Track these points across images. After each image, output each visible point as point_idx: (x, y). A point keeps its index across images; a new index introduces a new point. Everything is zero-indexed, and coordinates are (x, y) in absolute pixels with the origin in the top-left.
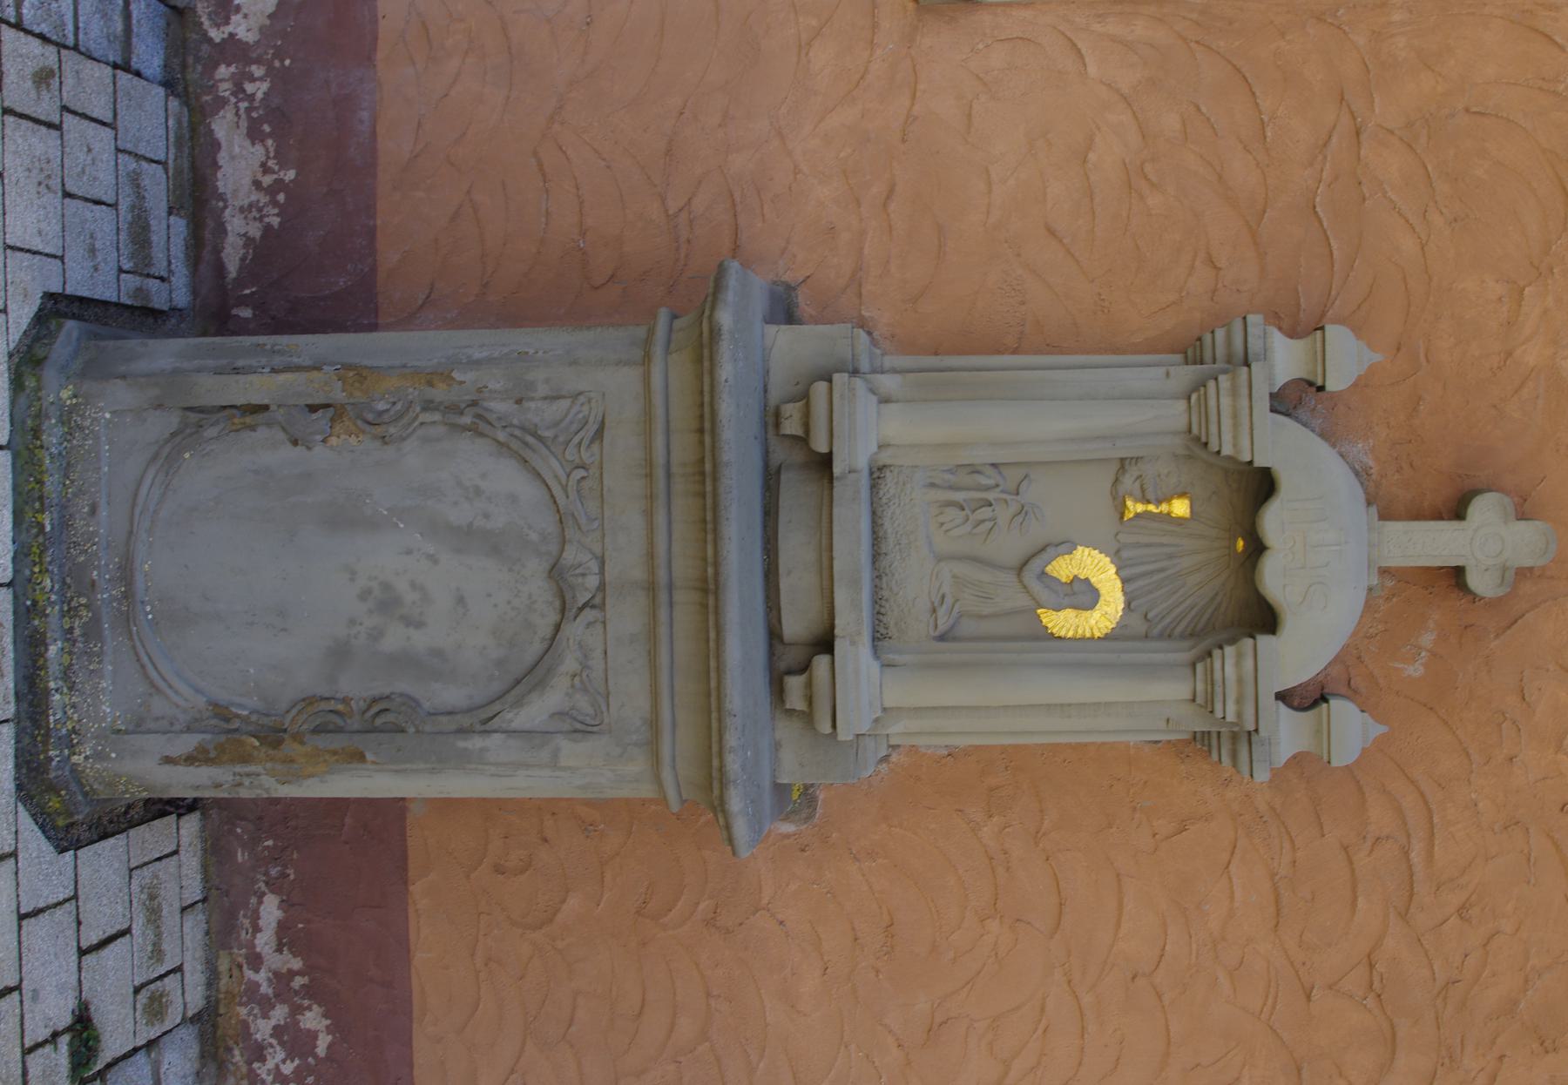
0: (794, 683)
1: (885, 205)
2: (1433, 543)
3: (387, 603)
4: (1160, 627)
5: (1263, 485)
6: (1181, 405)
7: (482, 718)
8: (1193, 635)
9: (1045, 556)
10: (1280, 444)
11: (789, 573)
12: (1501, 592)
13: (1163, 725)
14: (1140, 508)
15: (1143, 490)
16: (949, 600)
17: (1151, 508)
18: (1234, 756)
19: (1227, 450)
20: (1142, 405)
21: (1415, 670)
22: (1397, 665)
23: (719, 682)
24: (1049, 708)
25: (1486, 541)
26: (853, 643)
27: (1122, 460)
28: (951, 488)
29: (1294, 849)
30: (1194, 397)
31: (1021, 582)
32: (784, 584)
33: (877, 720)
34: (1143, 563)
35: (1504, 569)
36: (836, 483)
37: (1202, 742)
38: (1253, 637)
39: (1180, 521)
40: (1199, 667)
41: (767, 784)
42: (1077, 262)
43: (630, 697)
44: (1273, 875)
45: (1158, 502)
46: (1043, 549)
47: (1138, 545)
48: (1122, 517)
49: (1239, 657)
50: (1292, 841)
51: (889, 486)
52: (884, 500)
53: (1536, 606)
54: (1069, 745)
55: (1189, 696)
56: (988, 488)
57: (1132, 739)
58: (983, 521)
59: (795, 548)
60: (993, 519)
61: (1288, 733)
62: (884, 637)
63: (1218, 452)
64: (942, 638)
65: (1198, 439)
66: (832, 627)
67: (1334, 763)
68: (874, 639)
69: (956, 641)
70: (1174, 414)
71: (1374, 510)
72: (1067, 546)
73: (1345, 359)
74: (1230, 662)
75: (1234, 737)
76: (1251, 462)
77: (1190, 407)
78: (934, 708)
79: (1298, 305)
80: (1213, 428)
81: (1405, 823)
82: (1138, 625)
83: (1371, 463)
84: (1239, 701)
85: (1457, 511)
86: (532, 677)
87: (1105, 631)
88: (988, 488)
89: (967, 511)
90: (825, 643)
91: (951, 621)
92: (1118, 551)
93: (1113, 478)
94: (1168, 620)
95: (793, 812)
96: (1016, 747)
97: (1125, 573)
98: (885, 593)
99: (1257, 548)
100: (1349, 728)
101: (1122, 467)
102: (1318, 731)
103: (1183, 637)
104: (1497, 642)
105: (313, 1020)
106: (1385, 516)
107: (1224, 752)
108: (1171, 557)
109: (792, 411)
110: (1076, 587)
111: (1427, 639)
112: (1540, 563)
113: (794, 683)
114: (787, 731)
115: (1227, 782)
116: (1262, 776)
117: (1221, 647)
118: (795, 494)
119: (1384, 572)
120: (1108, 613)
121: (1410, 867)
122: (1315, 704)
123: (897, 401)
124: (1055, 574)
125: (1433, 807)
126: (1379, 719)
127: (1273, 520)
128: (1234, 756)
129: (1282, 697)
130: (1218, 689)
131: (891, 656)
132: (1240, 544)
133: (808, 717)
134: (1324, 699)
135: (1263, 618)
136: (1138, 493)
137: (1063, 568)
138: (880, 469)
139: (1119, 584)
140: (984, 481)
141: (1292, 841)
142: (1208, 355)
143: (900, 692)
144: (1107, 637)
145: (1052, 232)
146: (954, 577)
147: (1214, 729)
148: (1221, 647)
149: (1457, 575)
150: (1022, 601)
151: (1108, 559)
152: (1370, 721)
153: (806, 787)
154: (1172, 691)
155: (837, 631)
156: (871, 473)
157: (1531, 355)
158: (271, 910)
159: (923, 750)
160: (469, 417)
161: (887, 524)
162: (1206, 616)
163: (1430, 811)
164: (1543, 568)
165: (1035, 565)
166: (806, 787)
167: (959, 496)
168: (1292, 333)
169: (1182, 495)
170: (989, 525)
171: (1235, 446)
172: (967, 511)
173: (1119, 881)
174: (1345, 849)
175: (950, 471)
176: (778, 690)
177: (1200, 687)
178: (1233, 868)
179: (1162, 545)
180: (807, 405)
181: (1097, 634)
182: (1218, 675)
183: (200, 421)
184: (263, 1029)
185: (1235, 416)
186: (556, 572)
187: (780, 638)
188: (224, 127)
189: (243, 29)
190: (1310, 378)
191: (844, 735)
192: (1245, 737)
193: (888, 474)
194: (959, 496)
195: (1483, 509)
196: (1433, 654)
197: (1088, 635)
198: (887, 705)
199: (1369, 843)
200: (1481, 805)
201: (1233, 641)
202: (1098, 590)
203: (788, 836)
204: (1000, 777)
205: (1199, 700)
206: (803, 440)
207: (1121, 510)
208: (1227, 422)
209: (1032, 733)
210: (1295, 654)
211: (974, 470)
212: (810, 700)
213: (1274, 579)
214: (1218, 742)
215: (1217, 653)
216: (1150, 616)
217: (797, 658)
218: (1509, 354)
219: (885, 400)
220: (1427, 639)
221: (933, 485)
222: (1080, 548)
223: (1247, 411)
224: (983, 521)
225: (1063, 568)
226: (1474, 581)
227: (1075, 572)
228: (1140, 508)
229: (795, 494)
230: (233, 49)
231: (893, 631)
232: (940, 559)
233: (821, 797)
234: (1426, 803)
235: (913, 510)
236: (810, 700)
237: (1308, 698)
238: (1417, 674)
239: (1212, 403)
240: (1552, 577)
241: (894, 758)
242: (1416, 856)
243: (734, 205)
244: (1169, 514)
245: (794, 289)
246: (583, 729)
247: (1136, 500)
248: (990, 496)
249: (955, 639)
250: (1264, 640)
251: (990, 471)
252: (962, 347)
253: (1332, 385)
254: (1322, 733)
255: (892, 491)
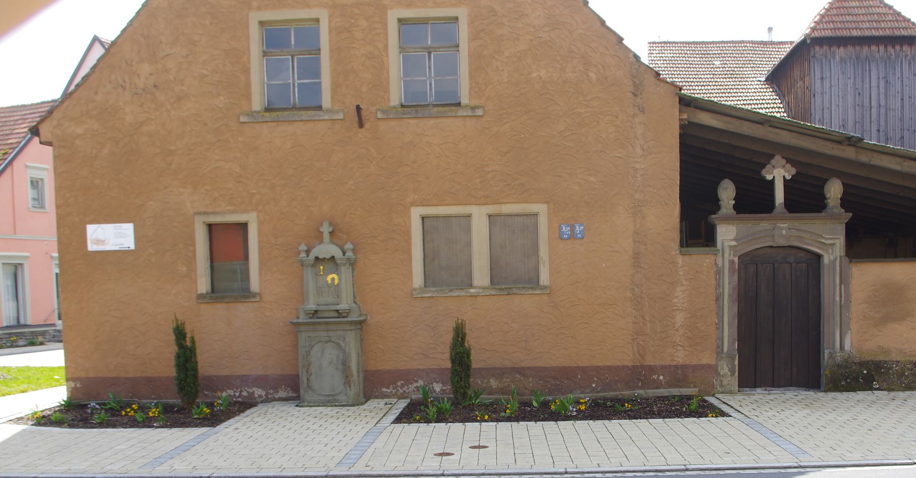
2: (326, 237)
3: (330, 363)
5: (317, 258)
7: (344, 351)
10: (312, 256)
20: (309, 273)
43: (340, 333)
59: (326, 315)
61: (349, 254)
69: (338, 296)
70: (309, 269)
73: (303, 247)
86: (338, 344)
90: (337, 311)
100: (349, 246)
105: (399, 384)
118: (320, 315)
120: (335, 276)
127: (321, 257)
137: (330, 282)
158: (384, 390)
160: (308, 353)
183: (309, 387)
184: (401, 391)
186: (326, 342)
188: (277, 397)
189: (264, 394)
195: (321, 230)
202: (332, 277)
210: (338, 253)
213: (328, 256)
214: (352, 264)
225: (330, 282)
229: (320, 315)
230: (266, 395)
246: (345, 339)
252: (303, 297)
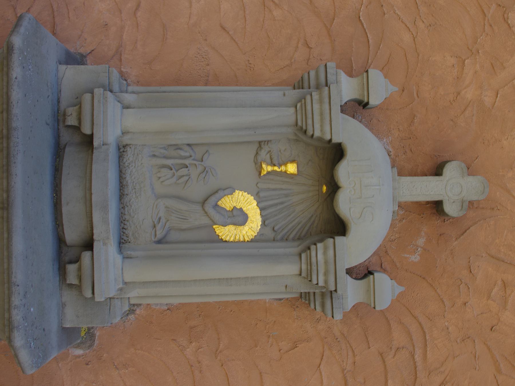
0: (72, 268)
1: (135, 14)
2: (426, 189)
4: (281, 234)
6: (292, 110)
8: (300, 238)
9: (217, 195)
11: (67, 204)
12: (461, 214)
13: (283, 289)
14: (270, 168)
15: (271, 159)
16: (163, 220)
17: (276, 168)
18: (323, 306)
19: (317, 134)
20: (270, 111)
21: (415, 258)
22: (406, 255)
23: (9, 265)
24: (220, 280)
25: (453, 187)
26: (105, 244)
27: (260, 143)
28: (166, 157)
29: (354, 356)
30: (299, 105)
31: (204, 210)
32: (65, 210)
33: (121, 290)
34: (272, 200)
35: (463, 202)
36: (94, 151)
37: (305, 298)
38: (334, 238)
39: (292, 175)
40: (303, 256)
41: (54, 327)
42: (236, 43)
44: (343, 370)
45: (280, 166)
46: (217, 192)
47: (269, 189)
48: (260, 174)
49: (326, 249)
50: (353, 352)
51: (129, 157)
52: (126, 164)
53: (475, 223)
54: (233, 302)
55: (298, 272)
56: (186, 158)
57: (267, 298)
58: (183, 176)
59: (71, 188)
60: (188, 175)
61: (352, 292)
62: (126, 242)
63: (313, 135)
64: (159, 242)
65: (302, 128)
66: (93, 235)
67: (378, 308)
68: (120, 243)
69: (166, 243)
70: (288, 115)
71: (395, 170)
72: (230, 190)
73: (380, 90)
74: (320, 252)
75: (323, 295)
76: (330, 140)
77: (296, 111)
78: (154, 282)
79: (352, 67)
80: (310, 121)
81: (412, 340)
82: (270, 234)
83: (390, 150)
84: (326, 274)
85: (437, 171)
87: (251, 237)
88: (186, 158)
89: (174, 170)
90: (89, 245)
91: (164, 233)
92: (258, 193)
93: (255, 152)
94: (286, 231)
95: (82, 343)
96: (205, 303)
97: (263, 204)
98: (127, 217)
99: (334, 188)
100: (385, 288)
101: (260, 146)
102: (368, 291)
103: (294, 240)
104: (456, 242)
106: (400, 174)
107: (317, 303)
108: (287, 196)
109: (72, 111)
110: (235, 213)
111: (421, 241)
112: (481, 198)
113: (72, 268)
114: (68, 296)
115: (318, 320)
116: (338, 316)
117: (315, 244)
119: (400, 206)
121: (415, 363)
122: (365, 276)
123: (134, 108)
124: (223, 206)
125: (426, 331)
126: (400, 283)
127: (344, 172)
128: (323, 306)
129: (349, 272)
130: (314, 268)
131: (129, 252)
132: (325, 188)
133: (79, 288)
134: (370, 273)
135: (339, 227)
136: (269, 160)
138: (124, 147)
139: (258, 211)
140: (183, 153)
141: (353, 352)
142: (306, 84)
143: (132, 274)
144: (252, 241)
145: (224, 29)
146: (166, 207)
147: (312, 291)
148: (315, 244)
149: (437, 206)
150: (205, 221)
151: (252, 197)
152: (396, 284)
153: (89, 329)
154: (288, 269)
155: (94, 237)
156: (119, 149)
157: (470, 94)
159: (154, 307)
161: (128, 178)
162: (306, 228)
163: (424, 333)
164: (478, 201)
165: (212, 200)
166: (89, 329)
167: (169, 162)
168: (350, 74)
169: (292, 161)
170: (186, 178)
171: (321, 131)
172: (174, 170)
173: (261, 376)
174: (381, 354)
175: (164, 148)
176: (62, 272)
177: (304, 267)
178: (322, 367)
179: (282, 189)
180: (80, 107)
181: (247, 239)
182: (314, 260)
185: (321, 114)
187: (65, 242)
190: (360, 98)
191: (98, 299)
192: (330, 295)
193: (128, 149)
194: (169, 162)
195: (450, 170)
196: (425, 250)
197: (242, 239)
198: (126, 280)
199: (393, 351)
200: (450, 328)
201: (321, 241)
202: (246, 214)
203: (79, 357)
204: (195, 320)
205: (304, 274)
206: (77, 128)
207: (260, 169)
208: (317, 118)
209: (210, 295)
210: (358, 246)
211: (177, 147)
212: (80, 278)
213: (345, 205)
214: (314, 298)
215: (313, 247)
216: (276, 229)
217: (71, 253)
218: (459, 94)
219: (127, 107)
220: (421, 241)
221: (154, 156)
222: (237, 192)
223: (328, 111)
224: (183, 176)
226: (448, 208)
227: (235, 205)
228: (270, 168)
231: (131, 238)
232: (158, 197)
233: (98, 334)
234: (422, 328)
235: (142, 169)
236: (80, 278)
237: (363, 273)
238: (417, 260)
239: (309, 107)
240: (483, 208)
241: (138, 312)
242: (418, 357)
243: (53, 11)
244: (285, 172)
245: (85, 57)
247: (268, 164)
248: (187, 162)
249: (167, 243)
250: (339, 239)
251: (187, 148)
252: (171, 82)
253: (374, 101)
254: (371, 292)
255: (131, 159)
